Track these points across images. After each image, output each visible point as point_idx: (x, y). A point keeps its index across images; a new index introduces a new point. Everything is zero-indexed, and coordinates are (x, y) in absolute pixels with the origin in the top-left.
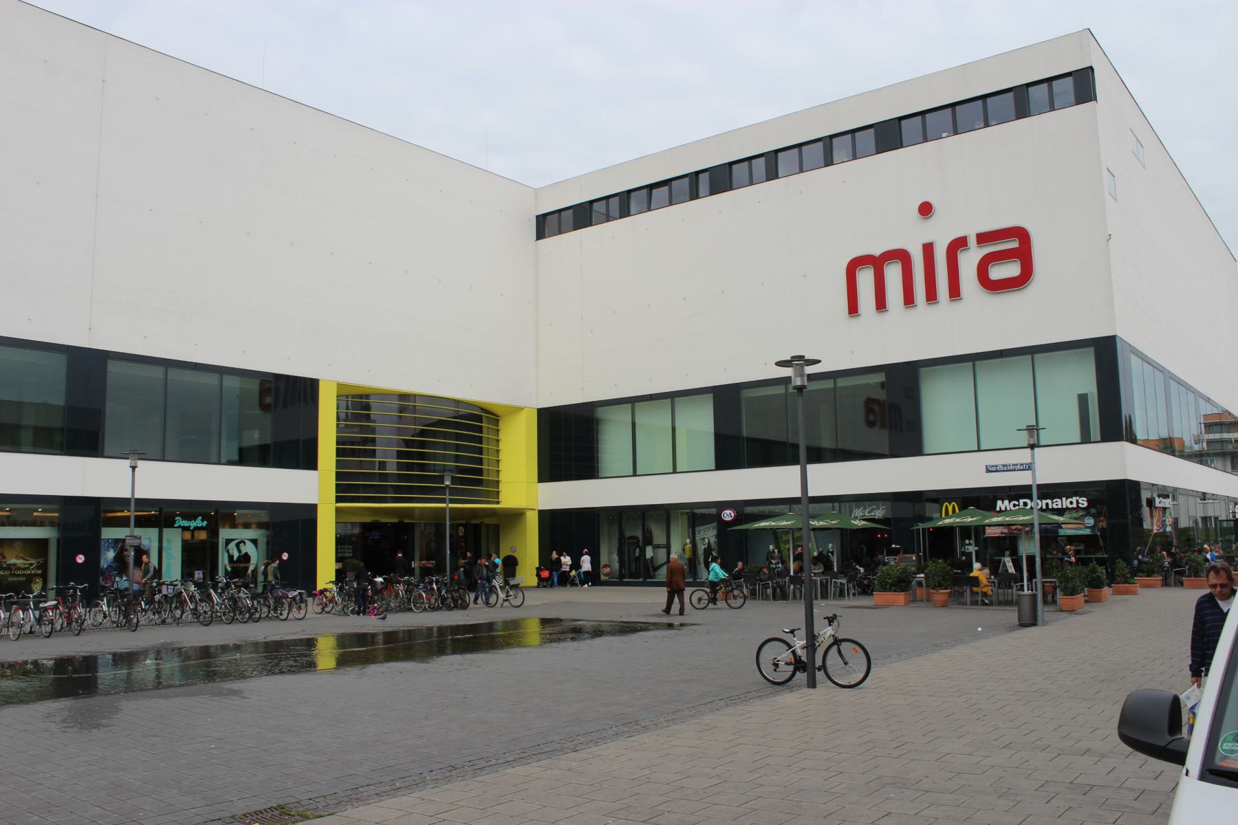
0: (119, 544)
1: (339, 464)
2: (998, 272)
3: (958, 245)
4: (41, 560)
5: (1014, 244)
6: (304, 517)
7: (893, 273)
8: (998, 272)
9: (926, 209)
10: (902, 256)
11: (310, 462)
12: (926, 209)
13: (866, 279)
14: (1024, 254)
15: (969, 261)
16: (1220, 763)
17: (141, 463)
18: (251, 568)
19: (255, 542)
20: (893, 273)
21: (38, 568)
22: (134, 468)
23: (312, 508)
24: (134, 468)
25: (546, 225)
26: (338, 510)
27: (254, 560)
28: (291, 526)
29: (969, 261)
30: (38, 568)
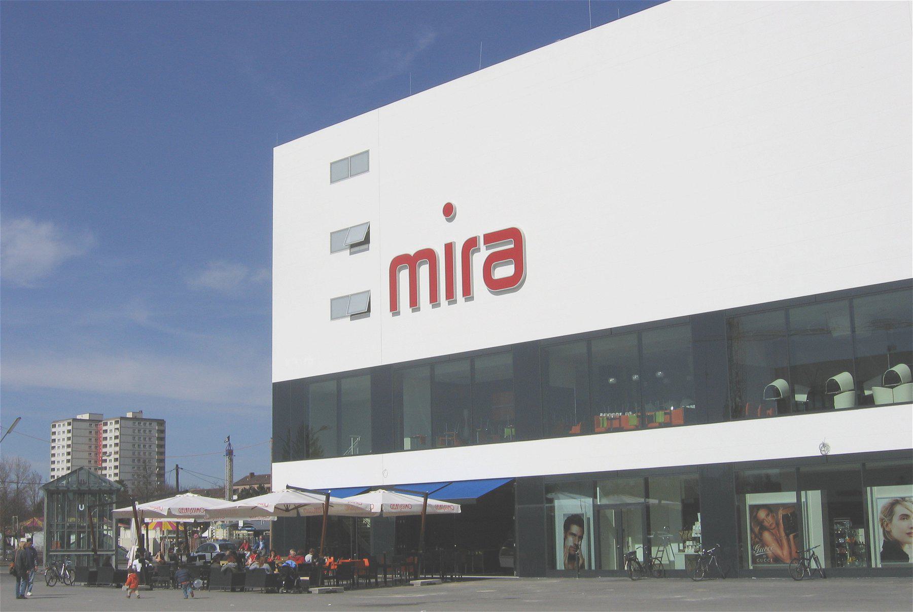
3: (471, 245)
7: (424, 271)
9: (449, 210)
10: (428, 255)
12: (449, 210)
13: (404, 276)
14: (517, 255)
20: (424, 271)
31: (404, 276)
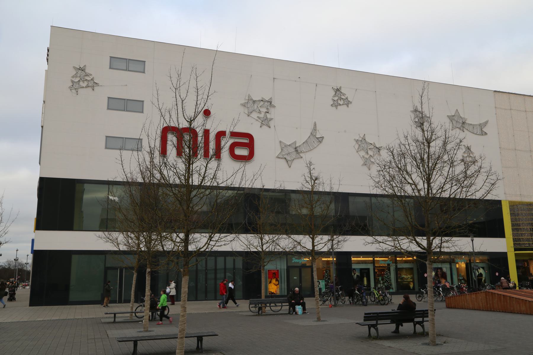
0: (436, 270)
1: (514, 235)
2: (239, 152)
3: (221, 134)
4: (412, 276)
5: (246, 141)
6: (502, 258)
8: (239, 152)
11: (501, 234)
15: (226, 143)
16: (303, 269)
17: (475, 239)
18: (483, 279)
19: (483, 268)
21: (411, 278)
22: (472, 240)
23: (506, 254)
24: (472, 240)
25: (315, 124)
26: (516, 255)
27: (484, 276)
28: (497, 261)
29: (226, 143)
30: (411, 278)
31: (172, 139)
